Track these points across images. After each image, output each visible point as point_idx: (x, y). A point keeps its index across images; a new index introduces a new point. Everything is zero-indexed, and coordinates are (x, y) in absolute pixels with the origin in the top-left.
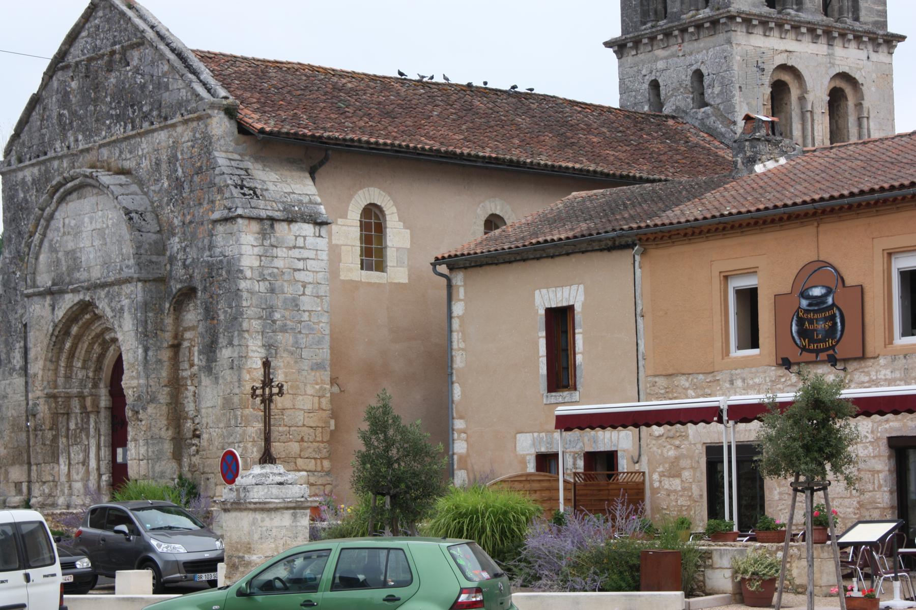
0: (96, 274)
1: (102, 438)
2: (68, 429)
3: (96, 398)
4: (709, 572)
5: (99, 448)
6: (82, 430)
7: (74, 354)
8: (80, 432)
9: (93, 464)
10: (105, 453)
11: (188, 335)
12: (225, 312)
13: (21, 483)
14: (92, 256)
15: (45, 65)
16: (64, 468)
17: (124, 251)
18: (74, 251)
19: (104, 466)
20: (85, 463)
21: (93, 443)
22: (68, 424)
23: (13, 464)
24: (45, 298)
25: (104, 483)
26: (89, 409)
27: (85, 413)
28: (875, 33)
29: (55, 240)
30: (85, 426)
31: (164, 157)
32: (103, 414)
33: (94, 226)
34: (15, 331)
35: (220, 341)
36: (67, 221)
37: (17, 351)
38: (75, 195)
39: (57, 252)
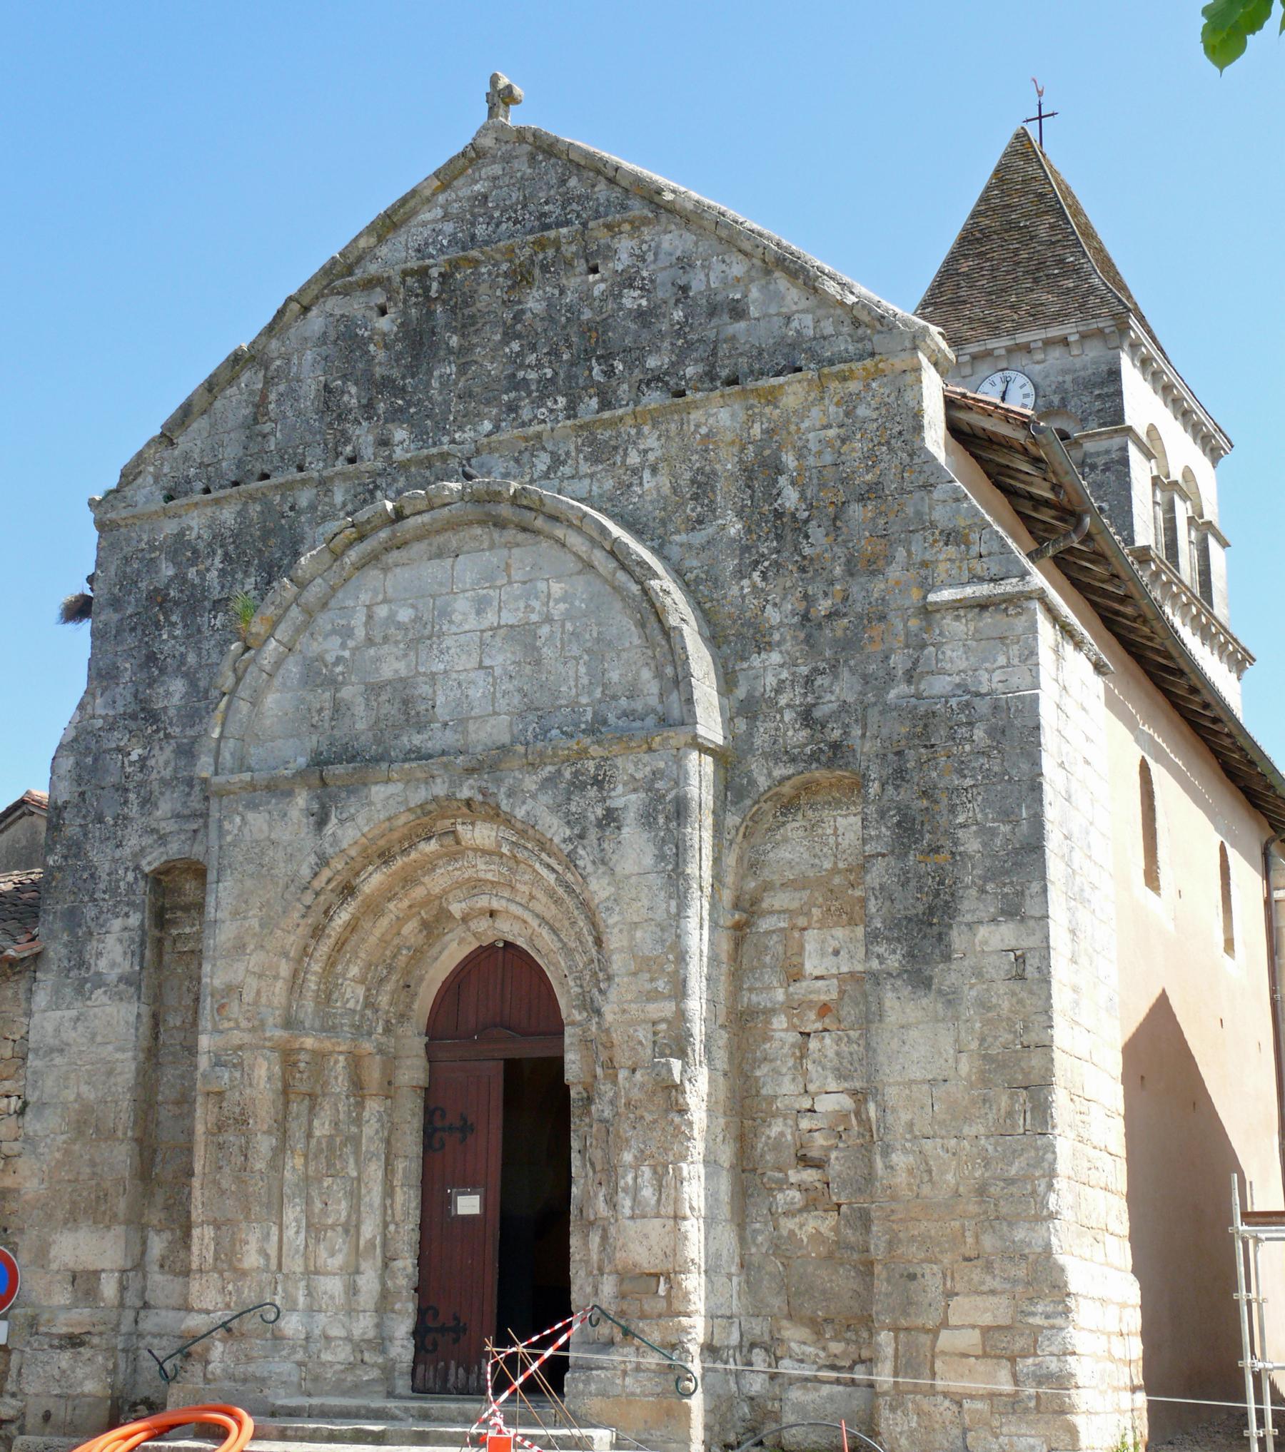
0: (492, 730)
1: (400, 1165)
2: (309, 1135)
3: (391, 1060)
5: (389, 1192)
9: (369, 1229)
11: (779, 900)
12: (987, 834)
13: (96, 1274)
16: (295, 1236)
18: (404, 682)
20: (351, 1228)
21: (375, 1171)
22: (310, 1123)
23: (71, 1221)
24: (290, 794)
27: (357, 1085)
28: (630, 730)
29: (330, 658)
30: (354, 1129)
31: (727, 464)
33: (491, 618)
34: (113, 890)
35: (965, 905)
36: (382, 612)
37: (111, 940)
38: (418, 548)
39: (333, 683)
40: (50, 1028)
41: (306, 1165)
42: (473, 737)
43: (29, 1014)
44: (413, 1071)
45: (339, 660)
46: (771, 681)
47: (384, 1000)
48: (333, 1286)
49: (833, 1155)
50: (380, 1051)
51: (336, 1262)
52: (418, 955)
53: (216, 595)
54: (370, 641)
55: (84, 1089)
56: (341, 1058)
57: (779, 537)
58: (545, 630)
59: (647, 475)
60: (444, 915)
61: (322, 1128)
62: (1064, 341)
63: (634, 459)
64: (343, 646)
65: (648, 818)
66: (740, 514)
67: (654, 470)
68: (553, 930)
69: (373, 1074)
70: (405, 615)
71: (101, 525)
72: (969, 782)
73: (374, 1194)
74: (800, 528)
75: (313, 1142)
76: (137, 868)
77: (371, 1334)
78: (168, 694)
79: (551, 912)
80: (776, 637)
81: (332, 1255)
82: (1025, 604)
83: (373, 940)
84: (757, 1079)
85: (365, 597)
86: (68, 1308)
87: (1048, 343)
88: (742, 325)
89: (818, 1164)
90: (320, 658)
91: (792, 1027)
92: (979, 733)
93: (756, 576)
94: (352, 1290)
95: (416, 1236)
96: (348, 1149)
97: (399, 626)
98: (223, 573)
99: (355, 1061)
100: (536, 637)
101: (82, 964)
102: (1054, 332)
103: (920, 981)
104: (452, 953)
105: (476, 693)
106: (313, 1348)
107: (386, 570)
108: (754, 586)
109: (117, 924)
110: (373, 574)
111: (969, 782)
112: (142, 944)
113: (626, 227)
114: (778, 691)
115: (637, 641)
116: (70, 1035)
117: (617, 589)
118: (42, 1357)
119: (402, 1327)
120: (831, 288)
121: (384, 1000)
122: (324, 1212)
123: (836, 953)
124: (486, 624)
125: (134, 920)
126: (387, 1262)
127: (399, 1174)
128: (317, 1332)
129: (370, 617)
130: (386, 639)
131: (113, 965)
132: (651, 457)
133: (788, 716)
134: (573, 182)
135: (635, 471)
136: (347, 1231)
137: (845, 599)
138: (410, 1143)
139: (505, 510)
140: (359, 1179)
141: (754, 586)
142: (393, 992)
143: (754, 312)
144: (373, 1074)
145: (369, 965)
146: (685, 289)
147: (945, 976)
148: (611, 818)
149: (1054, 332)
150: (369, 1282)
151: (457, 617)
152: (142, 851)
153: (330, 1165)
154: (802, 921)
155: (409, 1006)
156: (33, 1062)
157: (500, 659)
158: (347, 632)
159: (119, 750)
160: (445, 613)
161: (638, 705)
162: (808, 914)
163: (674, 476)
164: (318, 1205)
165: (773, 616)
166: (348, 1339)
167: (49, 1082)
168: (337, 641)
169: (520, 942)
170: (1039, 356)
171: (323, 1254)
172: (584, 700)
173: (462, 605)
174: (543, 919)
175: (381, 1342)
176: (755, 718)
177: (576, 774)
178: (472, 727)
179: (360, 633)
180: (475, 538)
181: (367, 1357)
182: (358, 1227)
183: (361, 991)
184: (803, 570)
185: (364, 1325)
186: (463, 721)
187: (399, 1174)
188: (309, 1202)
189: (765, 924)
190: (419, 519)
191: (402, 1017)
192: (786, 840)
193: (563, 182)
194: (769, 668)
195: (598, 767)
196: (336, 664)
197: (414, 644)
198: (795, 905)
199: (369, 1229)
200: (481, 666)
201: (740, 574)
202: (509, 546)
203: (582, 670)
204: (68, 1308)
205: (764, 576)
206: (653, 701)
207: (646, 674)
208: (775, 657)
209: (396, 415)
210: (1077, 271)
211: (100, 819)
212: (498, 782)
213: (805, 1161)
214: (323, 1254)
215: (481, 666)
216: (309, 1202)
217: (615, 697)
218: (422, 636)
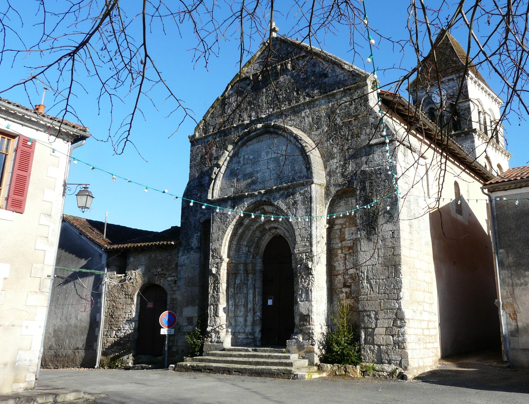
1: (257, 290)
2: (235, 283)
3: (254, 264)
4: (477, 160)
5: (254, 297)
6: (244, 283)
7: (242, 237)
8: (243, 286)
9: (250, 306)
10: (258, 298)
11: (338, 221)
14: (267, 175)
15: (128, 371)
17: (296, 168)
19: (258, 307)
20: (246, 305)
21: (251, 292)
22: (235, 280)
23: (187, 305)
24: (227, 202)
25: (258, 318)
26: (250, 272)
27: (246, 272)
29: (236, 169)
30: (246, 282)
32: (258, 275)
33: (270, 156)
36: (246, 157)
37: (194, 239)
38: (254, 140)
40: (182, 260)
41: (234, 291)
42: (266, 185)
43: (178, 257)
44: (259, 266)
45: (238, 169)
46: (335, 166)
47: (252, 250)
48: (241, 320)
49: (353, 284)
50: (252, 263)
51: (242, 314)
52: (260, 239)
53: (215, 156)
54: (244, 164)
55: (189, 274)
56: (242, 265)
57: (336, 131)
58: (281, 158)
59: (306, 118)
60: (265, 230)
61: (238, 281)
62: (453, 79)
63: (303, 114)
64: (238, 166)
65: (304, 203)
66: (326, 125)
67: (308, 117)
68: (288, 232)
69: (250, 267)
70: (251, 157)
71: (191, 142)
72: (380, 188)
73: (251, 297)
74: (341, 128)
75: (236, 285)
76: (200, 221)
77: (250, 331)
78: (205, 180)
79: (286, 227)
80: (336, 155)
81: (240, 312)
82: (393, 142)
83: (249, 236)
84: (335, 266)
85: (243, 154)
86: (186, 326)
87: (449, 80)
88: (327, 79)
89: (349, 287)
90: (234, 169)
91: (342, 253)
92: (383, 176)
93: (331, 141)
94: (246, 321)
95: (261, 307)
96: (245, 286)
97: (250, 160)
98: (216, 151)
99: (246, 264)
100: (279, 160)
101: (189, 245)
102: (450, 77)
103: (369, 240)
104: (267, 238)
105: (267, 175)
106: (236, 334)
107: (247, 147)
108: (330, 143)
109: (195, 235)
110: (245, 148)
111: (380, 188)
112: (201, 240)
113: (301, 58)
114: (336, 169)
115: (301, 159)
116: (186, 262)
117: (297, 146)
118: (181, 337)
119: (258, 329)
120: (346, 67)
121: (252, 250)
122: (239, 302)
123: (352, 233)
124: (268, 158)
125: (199, 234)
126: (254, 314)
127: (257, 292)
128: (237, 331)
129: (244, 158)
130: (247, 163)
131: (195, 245)
132: (307, 114)
133: (339, 175)
134: (289, 49)
135: (304, 118)
136: (244, 306)
137: (351, 145)
138: (259, 284)
139: (272, 130)
140: (247, 294)
141: (330, 143)
142: (254, 248)
143: (330, 75)
144: (250, 267)
145: (248, 242)
146: (314, 71)
147: (374, 238)
148: (295, 203)
149: (450, 77)
150: (250, 318)
151: (262, 157)
152: (200, 218)
153: (240, 290)
154: (344, 226)
155: (258, 251)
156: (179, 268)
157: (272, 166)
158: (239, 162)
159: (195, 194)
160: (260, 156)
161: (302, 175)
162: (346, 224)
163: (313, 119)
164: (237, 300)
165: (335, 150)
166: (245, 332)
167: (182, 273)
168: (237, 164)
169: (282, 235)
170: (447, 84)
171: (238, 312)
172: (290, 174)
173: (263, 153)
174: (284, 228)
175: (253, 333)
176: (331, 176)
177: (288, 193)
178: (266, 183)
179: (242, 162)
180: (266, 137)
181: (249, 336)
182: (247, 305)
183: (247, 249)
184: (341, 138)
185: (248, 329)
186: (264, 182)
187: (257, 292)
188: (235, 299)
189: (336, 227)
190: (253, 134)
191: (257, 254)
192: (340, 206)
193: (287, 49)
194: (334, 163)
195: (292, 191)
196: (237, 170)
197: (253, 164)
198: (343, 222)
199: (250, 306)
200: (268, 168)
201: (327, 140)
202: (273, 138)
203: (290, 167)
204: (186, 326)
205: (333, 141)
206: (305, 174)
207: (304, 167)
208: (335, 161)
209: (252, 109)
210: (456, 62)
211: (192, 211)
212: (271, 196)
213: (345, 286)
214: (238, 312)
215: (268, 168)
216: (235, 299)
217: (297, 173)
218: (255, 162)
